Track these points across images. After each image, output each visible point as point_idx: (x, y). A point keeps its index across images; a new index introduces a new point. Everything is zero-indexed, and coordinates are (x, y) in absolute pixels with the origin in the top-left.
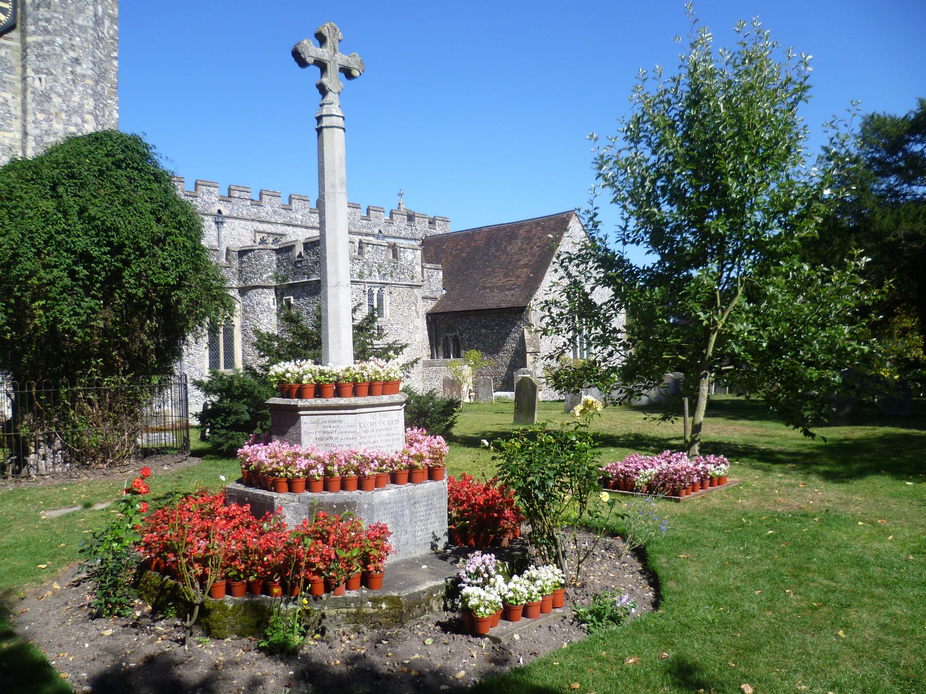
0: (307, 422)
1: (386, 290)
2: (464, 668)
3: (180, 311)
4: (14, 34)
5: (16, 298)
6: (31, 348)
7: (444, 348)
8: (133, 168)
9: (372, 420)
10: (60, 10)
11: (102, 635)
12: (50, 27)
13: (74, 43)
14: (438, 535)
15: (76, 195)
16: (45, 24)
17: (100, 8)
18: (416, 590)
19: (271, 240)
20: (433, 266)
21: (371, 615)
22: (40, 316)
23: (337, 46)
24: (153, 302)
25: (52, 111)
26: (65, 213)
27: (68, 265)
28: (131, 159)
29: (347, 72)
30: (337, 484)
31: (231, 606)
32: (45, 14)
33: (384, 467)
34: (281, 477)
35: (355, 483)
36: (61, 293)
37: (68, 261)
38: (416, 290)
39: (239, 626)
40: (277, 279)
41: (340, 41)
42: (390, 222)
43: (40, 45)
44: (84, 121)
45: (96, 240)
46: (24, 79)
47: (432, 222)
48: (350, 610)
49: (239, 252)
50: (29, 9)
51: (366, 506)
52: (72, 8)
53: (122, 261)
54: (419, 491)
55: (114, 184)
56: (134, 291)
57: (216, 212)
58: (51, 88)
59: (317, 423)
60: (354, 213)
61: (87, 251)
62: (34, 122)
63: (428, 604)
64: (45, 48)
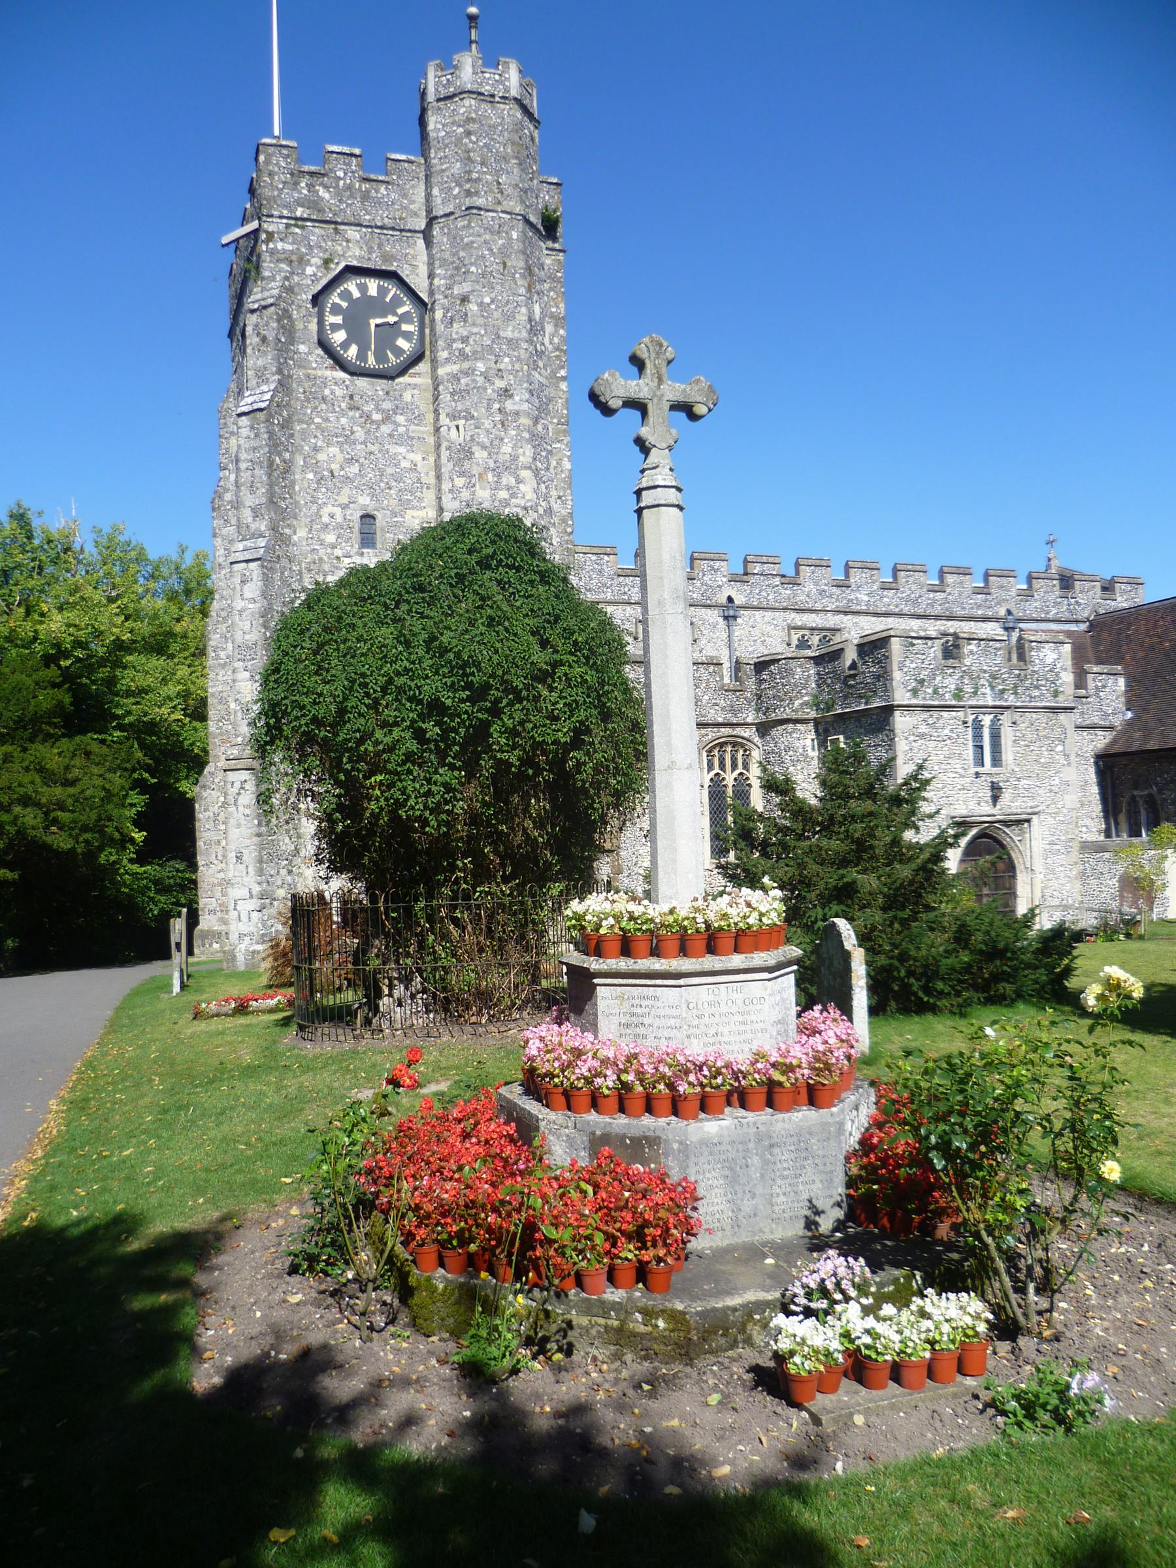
0: (606, 996)
1: (1006, 718)
2: (732, 1462)
3: (579, 784)
4: (423, 367)
5: (347, 773)
6: (373, 844)
7: (1129, 819)
8: (507, 566)
9: (711, 997)
10: (480, 321)
11: (285, 1301)
12: (468, 349)
13: (502, 366)
14: (820, 1204)
15: (423, 616)
16: (461, 346)
17: (537, 308)
18: (720, 1305)
19: (815, 640)
20: (1105, 668)
21: (642, 1336)
22: (377, 799)
23: (664, 370)
24: (538, 771)
25: (475, 472)
26: (407, 644)
27: (413, 721)
28: (503, 552)
29: (686, 409)
30: (640, 1104)
31: (441, 1286)
32: (460, 330)
33: (719, 1080)
34: (556, 1086)
35: (667, 1104)
36: (404, 763)
37: (411, 715)
38: (1062, 717)
39: (452, 1320)
40: (817, 705)
41: (669, 362)
42: (1028, 595)
43: (456, 378)
44: (519, 481)
45: (449, 681)
46: (437, 430)
47: (1108, 588)
48: (610, 1322)
49: (755, 664)
50: (440, 328)
51: (676, 1146)
52: (496, 315)
53: (488, 711)
54: (779, 1126)
55: (478, 594)
56: (505, 756)
57: (724, 600)
58: (472, 440)
59: (621, 998)
60: (961, 583)
61: (438, 699)
62: (451, 491)
63: (742, 1330)
64: (462, 381)
